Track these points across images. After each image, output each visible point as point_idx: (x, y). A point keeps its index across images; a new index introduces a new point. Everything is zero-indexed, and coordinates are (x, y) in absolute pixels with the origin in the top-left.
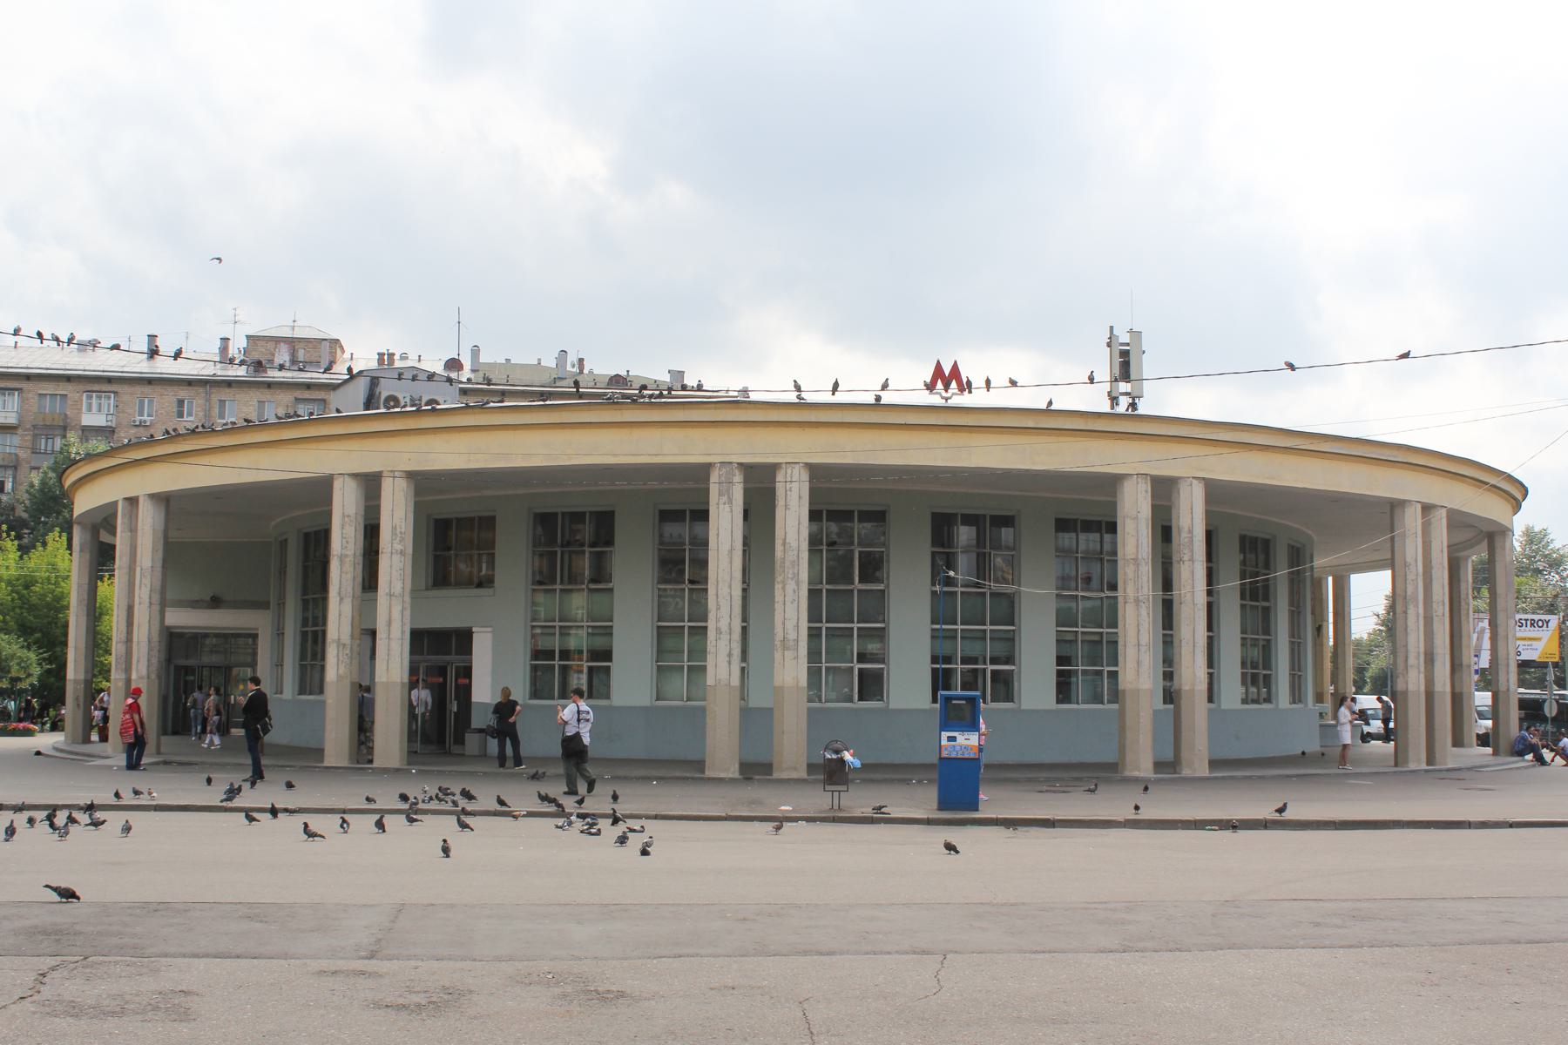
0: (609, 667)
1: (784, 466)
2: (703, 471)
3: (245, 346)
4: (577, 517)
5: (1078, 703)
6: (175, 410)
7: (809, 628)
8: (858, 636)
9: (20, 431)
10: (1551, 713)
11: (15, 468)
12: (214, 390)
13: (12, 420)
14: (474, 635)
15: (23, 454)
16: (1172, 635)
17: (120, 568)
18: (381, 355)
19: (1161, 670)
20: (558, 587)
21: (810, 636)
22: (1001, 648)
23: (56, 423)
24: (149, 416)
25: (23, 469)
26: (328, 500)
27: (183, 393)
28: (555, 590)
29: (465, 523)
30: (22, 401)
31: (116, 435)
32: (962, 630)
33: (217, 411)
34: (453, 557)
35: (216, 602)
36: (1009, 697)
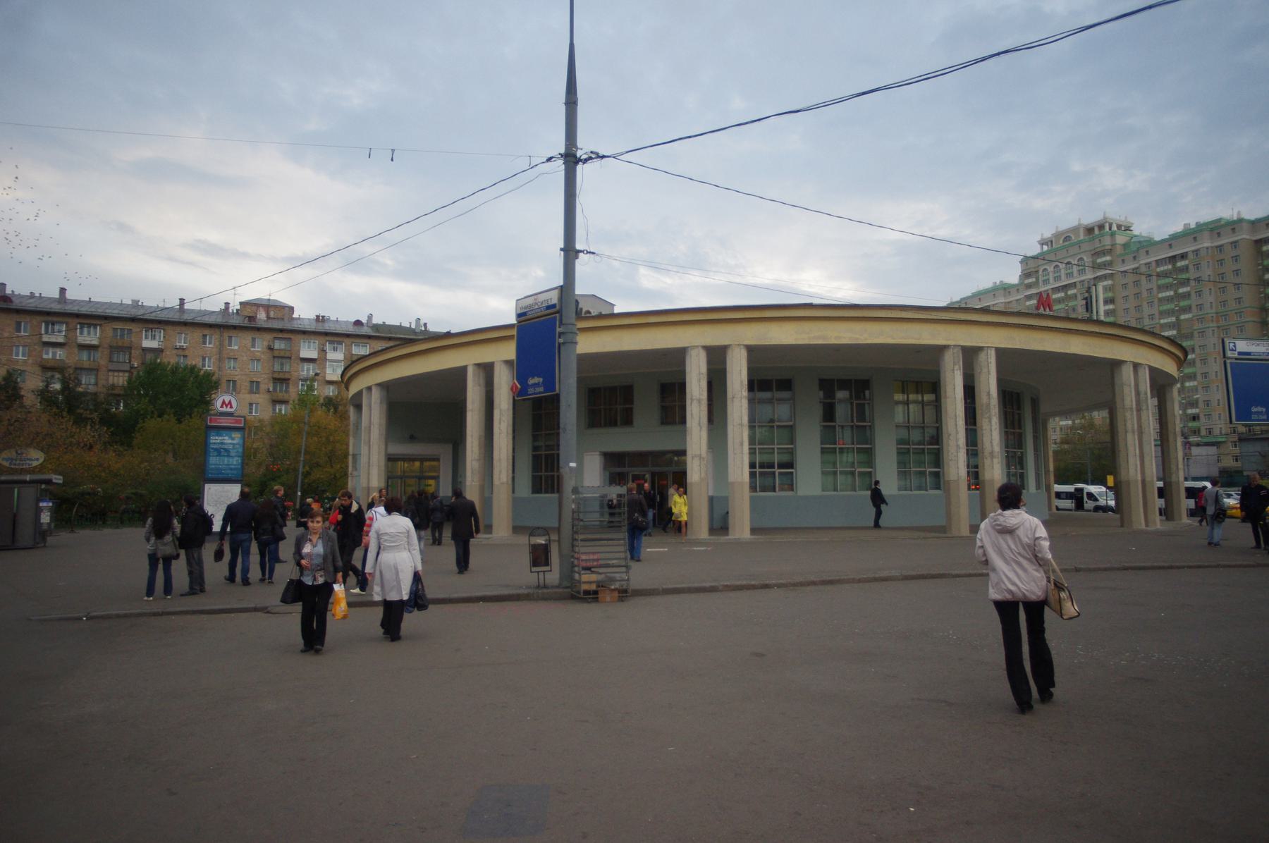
0: (792, 473)
1: (986, 349)
2: (942, 349)
4: (613, 390)
5: (911, 490)
6: (201, 340)
8: (759, 453)
9: (100, 349)
10: (60, 479)
11: (97, 370)
13: (95, 342)
16: (977, 450)
17: (472, 410)
18: (318, 317)
19: (980, 470)
21: (750, 453)
22: (785, 458)
23: (125, 345)
24: (184, 343)
26: (682, 363)
27: (207, 331)
30: (102, 331)
31: (164, 353)
35: (412, 438)
36: (791, 487)
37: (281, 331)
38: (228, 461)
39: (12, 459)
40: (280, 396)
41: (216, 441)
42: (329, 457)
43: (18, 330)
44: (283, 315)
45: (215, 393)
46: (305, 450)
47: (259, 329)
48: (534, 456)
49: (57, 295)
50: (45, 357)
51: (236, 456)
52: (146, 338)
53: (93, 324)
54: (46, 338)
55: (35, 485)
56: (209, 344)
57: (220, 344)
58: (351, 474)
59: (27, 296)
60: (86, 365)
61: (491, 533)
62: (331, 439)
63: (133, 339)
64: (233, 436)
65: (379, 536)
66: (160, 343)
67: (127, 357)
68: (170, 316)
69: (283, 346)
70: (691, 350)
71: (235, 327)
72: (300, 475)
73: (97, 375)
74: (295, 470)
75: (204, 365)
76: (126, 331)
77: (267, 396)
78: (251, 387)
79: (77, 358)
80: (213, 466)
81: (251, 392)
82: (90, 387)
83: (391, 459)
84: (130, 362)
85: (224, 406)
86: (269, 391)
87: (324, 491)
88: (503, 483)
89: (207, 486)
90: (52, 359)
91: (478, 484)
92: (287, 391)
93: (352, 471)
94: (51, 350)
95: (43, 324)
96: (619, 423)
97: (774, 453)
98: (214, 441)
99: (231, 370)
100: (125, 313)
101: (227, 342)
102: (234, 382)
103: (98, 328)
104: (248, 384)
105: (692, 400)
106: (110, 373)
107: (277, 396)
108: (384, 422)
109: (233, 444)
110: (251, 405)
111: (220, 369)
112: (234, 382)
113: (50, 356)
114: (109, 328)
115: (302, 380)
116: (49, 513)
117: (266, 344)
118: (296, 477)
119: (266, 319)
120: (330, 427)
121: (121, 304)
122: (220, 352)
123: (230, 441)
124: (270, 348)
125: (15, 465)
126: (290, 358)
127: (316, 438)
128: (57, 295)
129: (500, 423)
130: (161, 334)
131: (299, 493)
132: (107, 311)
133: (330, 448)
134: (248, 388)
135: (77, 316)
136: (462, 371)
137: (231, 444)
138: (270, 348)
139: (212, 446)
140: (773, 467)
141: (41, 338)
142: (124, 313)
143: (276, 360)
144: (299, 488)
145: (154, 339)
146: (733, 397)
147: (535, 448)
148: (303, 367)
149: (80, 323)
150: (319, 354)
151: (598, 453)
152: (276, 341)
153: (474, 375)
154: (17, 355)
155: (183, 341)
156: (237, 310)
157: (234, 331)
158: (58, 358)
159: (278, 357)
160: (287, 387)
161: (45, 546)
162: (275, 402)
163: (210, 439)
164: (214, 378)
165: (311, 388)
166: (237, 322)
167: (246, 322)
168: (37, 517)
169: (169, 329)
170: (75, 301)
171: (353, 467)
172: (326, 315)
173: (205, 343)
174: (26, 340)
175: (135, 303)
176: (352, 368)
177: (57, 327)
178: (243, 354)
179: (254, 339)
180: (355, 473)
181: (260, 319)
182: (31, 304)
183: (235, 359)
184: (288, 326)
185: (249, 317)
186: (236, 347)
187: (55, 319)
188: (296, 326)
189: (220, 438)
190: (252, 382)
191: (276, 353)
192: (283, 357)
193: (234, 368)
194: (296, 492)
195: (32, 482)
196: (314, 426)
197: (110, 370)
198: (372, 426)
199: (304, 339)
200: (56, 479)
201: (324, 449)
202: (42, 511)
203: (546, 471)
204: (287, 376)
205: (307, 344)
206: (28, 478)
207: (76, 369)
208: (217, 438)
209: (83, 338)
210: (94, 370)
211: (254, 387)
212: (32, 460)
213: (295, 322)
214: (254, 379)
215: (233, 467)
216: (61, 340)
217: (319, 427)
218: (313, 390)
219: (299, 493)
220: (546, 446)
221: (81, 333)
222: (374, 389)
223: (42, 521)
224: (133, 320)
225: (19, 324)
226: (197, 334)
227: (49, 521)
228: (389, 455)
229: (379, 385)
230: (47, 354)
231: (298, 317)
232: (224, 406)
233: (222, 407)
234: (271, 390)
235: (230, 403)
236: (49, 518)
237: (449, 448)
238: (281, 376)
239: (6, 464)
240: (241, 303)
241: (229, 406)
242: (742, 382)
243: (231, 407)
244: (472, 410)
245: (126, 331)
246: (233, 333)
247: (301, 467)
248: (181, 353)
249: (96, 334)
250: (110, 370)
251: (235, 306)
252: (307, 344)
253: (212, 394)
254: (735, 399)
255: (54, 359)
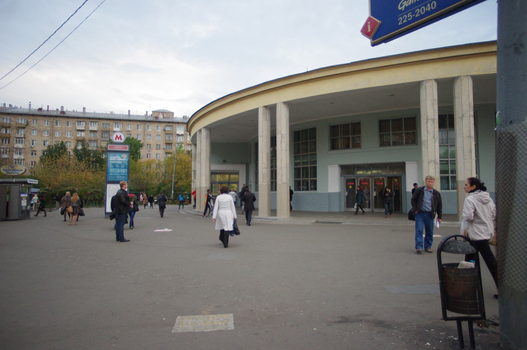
3: (152, 114)
6: (137, 127)
7: (440, 161)
8: (450, 164)
9: (98, 132)
12: (146, 123)
14: (406, 165)
15: (99, 138)
17: (262, 136)
18: (184, 116)
20: (309, 153)
23: (107, 130)
25: (99, 141)
27: (139, 123)
28: (300, 156)
29: (346, 126)
30: (98, 125)
32: (450, 161)
33: (147, 128)
34: (340, 138)
35: (225, 162)
37: (169, 122)
38: (120, 171)
39: (9, 170)
40: (169, 151)
41: (113, 159)
42: (186, 175)
43: (68, 125)
44: (170, 116)
45: (141, 149)
46: (175, 172)
47: (160, 122)
48: (295, 169)
49: (82, 111)
50: (78, 136)
51: (124, 168)
52: (115, 127)
53: (95, 122)
54: (78, 128)
55: (18, 184)
56: (140, 129)
57: (144, 129)
58: (193, 181)
59: (72, 111)
60: (93, 139)
61: (276, 215)
62: (187, 166)
63: (110, 128)
64: (123, 156)
65: (219, 203)
66: (121, 129)
67: (108, 135)
68: (124, 118)
69: (169, 129)
70: (426, 82)
71: (150, 121)
72: (173, 183)
73: (97, 143)
74: (171, 181)
75: (138, 138)
76: (105, 124)
77: (163, 151)
78: (157, 147)
79: (89, 136)
80: (112, 174)
81: (157, 149)
82: (94, 148)
83: (213, 173)
84: (109, 137)
85: (117, 139)
86: (164, 149)
87: (184, 191)
88: (284, 183)
89: (108, 185)
90: (80, 137)
91: (266, 183)
92: (171, 148)
93: (194, 179)
94: (80, 133)
95: (77, 122)
96: (351, 146)
97: (448, 164)
98: (112, 159)
99: (149, 140)
100: (107, 117)
101: (147, 128)
102: (150, 145)
103: (97, 123)
104: (156, 146)
105: (427, 120)
106: (102, 142)
107: (168, 151)
108: (208, 149)
109: (123, 161)
110: (157, 154)
111: (144, 139)
112: (150, 145)
113: (80, 135)
114: (101, 122)
115: (178, 144)
116: (26, 200)
117: (162, 128)
118: (171, 185)
119: (162, 118)
120: (186, 160)
121: (106, 113)
122: (144, 132)
123: (121, 159)
124: (164, 130)
125: (9, 173)
126: (172, 134)
127: (180, 166)
128: (82, 111)
129: (281, 143)
130: (121, 126)
131: (173, 192)
132: (100, 116)
133: (186, 171)
134: (156, 147)
135: (89, 118)
136: (255, 112)
137: (121, 161)
138: (164, 130)
139: (111, 162)
140: (448, 173)
141: (76, 128)
142: (107, 117)
143: (167, 135)
144: (173, 190)
145: (118, 127)
146: (463, 116)
147: (296, 164)
148: (178, 138)
149: (90, 122)
150: (184, 132)
151: (337, 165)
152: (167, 127)
153: (263, 113)
154: (68, 135)
155: (129, 128)
156: (151, 115)
157: (149, 123)
158: (82, 136)
159: (168, 134)
160: (172, 147)
161: (29, 218)
162: (167, 153)
163: (109, 158)
164: (141, 142)
165: (181, 147)
166: (151, 119)
167: (154, 119)
168: (20, 203)
169: (124, 123)
170: (89, 113)
171: (194, 177)
172: (187, 116)
173: (138, 128)
174: (71, 129)
175: (112, 113)
176: (192, 120)
177: (82, 123)
178: (153, 133)
179: (158, 126)
180: (195, 180)
181: (160, 118)
182: (72, 115)
183: (150, 135)
184: (171, 120)
185: (156, 117)
186: (151, 130)
187: (81, 120)
188: (175, 120)
189: (115, 157)
190: (157, 145)
191: (167, 132)
192: (170, 134)
193: (150, 139)
194: (172, 192)
195: (16, 183)
196: (179, 160)
197: (101, 141)
198: (202, 152)
199: (178, 126)
200: (29, 181)
201: (183, 171)
202: (22, 199)
203: (303, 178)
204: (171, 142)
205: (179, 128)
206: (14, 180)
207: (89, 140)
208: (113, 157)
209: (91, 128)
210: (96, 141)
211: (158, 146)
212: (19, 171)
213: (174, 119)
214: (158, 144)
215: (123, 174)
216: (83, 129)
217: (181, 161)
218: (182, 147)
219: (173, 192)
220: (303, 163)
221: (91, 126)
222: (203, 130)
223: (22, 205)
224: (110, 120)
225: (68, 123)
226: (134, 125)
227: (26, 205)
228: (211, 170)
229: (205, 127)
230: (78, 134)
231: (176, 117)
232: (117, 139)
233: (116, 139)
234: (165, 148)
235: (120, 137)
236: (26, 203)
237: (244, 166)
238: (169, 142)
239: (4, 172)
240: (153, 112)
241: (120, 139)
242: (470, 104)
243: (121, 139)
244: (262, 136)
245: (105, 124)
246: (149, 124)
247: (173, 180)
248: (129, 133)
249: (96, 126)
250: (101, 141)
251: (150, 113)
252: (179, 128)
253: (140, 150)
254: (464, 118)
255: (81, 137)
